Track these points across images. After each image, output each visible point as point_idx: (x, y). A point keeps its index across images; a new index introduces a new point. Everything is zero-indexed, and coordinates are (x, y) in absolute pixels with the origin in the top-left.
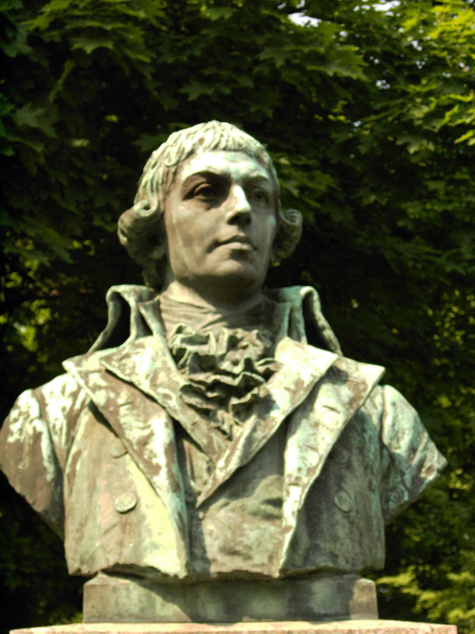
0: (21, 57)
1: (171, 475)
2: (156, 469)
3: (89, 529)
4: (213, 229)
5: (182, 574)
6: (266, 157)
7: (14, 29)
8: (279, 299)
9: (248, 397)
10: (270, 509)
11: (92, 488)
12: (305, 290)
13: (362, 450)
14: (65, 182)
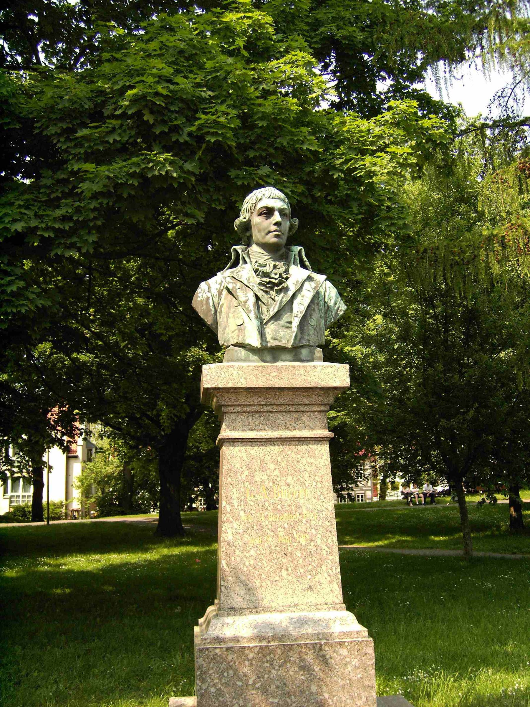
0: (186, 142)
1: (255, 313)
2: (250, 311)
3: (227, 331)
4: (269, 226)
5: (259, 347)
6: (287, 200)
7: (182, 130)
8: (290, 250)
9: (280, 287)
10: (288, 325)
11: (228, 317)
12: (299, 248)
13: (318, 304)
14: (202, 190)
